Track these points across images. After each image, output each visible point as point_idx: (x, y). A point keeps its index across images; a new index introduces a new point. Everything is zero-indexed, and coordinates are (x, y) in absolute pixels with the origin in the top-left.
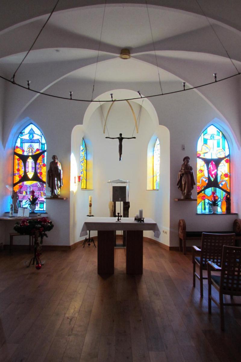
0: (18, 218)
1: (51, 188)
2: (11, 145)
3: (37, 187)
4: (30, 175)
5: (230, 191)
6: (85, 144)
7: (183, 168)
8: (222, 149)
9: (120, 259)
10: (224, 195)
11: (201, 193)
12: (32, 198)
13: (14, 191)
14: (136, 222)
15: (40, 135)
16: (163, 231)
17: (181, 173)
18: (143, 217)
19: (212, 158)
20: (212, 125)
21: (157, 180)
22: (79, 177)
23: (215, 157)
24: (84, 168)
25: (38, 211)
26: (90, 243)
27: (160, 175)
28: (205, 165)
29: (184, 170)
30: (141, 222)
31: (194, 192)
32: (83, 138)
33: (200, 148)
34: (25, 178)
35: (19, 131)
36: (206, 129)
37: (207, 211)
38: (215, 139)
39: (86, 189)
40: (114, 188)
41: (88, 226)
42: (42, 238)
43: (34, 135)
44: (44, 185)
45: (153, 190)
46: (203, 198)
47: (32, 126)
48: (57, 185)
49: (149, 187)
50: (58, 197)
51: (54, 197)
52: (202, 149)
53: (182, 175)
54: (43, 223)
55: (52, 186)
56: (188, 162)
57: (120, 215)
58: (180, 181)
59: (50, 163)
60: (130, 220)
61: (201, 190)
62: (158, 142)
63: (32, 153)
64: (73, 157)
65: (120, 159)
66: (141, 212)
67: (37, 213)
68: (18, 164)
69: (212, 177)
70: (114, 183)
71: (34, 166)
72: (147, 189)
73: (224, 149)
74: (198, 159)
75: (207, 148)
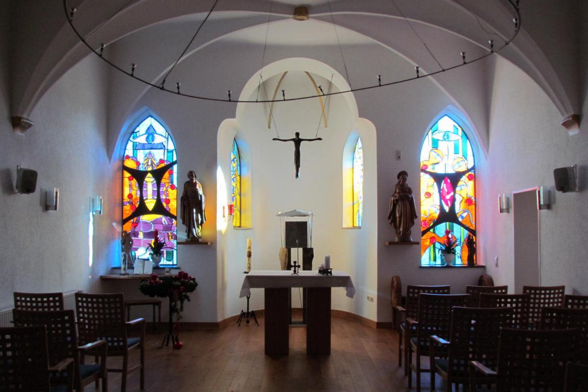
0: (135, 276)
1: (186, 225)
2: (118, 155)
3: (162, 224)
4: (150, 204)
5: (475, 228)
6: (238, 149)
7: (397, 191)
8: (462, 157)
9: (298, 339)
10: (465, 234)
11: (428, 233)
12: (154, 244)
13: (124, 232)
14: (320, 275)
15: (165, 135)
16: (368, 298)
17: (395, 199)
18: (331, 267)
19: (446, 173)
20: (446, 115)
21: (358, 211)
22: (231, 208)
23: (451, 171)
24: (237, 191)
25: (163, 265)
26: (250, 320)
27: (363, 202)
28: (435, 184)
29: (399, 193)
30: (327, 274)
31: (415, 231)
32: (235, 139)
33: (426, 155)
34: (142, 209)
35: (131, 131)
36: (437, 122)
37: (438, 263)
38: (450, 139)
39: (240, 227)
40: (287, 223)
41: (252, 281)
42: (182, 302)
43: (155, 135)
44: (173, 221)
45: (354, 227)
46: (433, 240)
47: (149, 121)
48: (197, 220)
49: (347, 223)
50: (198, 240)
51: (193, 240)
52: (429, 157)
53: (395, 202)
54: (183, 280)
55: (188, 222)
56: (405, 180)
57: (297, 264)
58: (393, 212)
59: (185, 184)
60: (314, 272)
61: (428, 227)
62: (360, 145)
63: (153, 166)
64: (220, 173)
65: (297, 176)
66: (328, 260)
67: (164, 268)
68: (130, 188)
69: (447, 204)
70: (288, 216)
71: (156, 189)
72: (344, 226)
73: (465, 157)
74: (422, 174)
75: (438, 155)
